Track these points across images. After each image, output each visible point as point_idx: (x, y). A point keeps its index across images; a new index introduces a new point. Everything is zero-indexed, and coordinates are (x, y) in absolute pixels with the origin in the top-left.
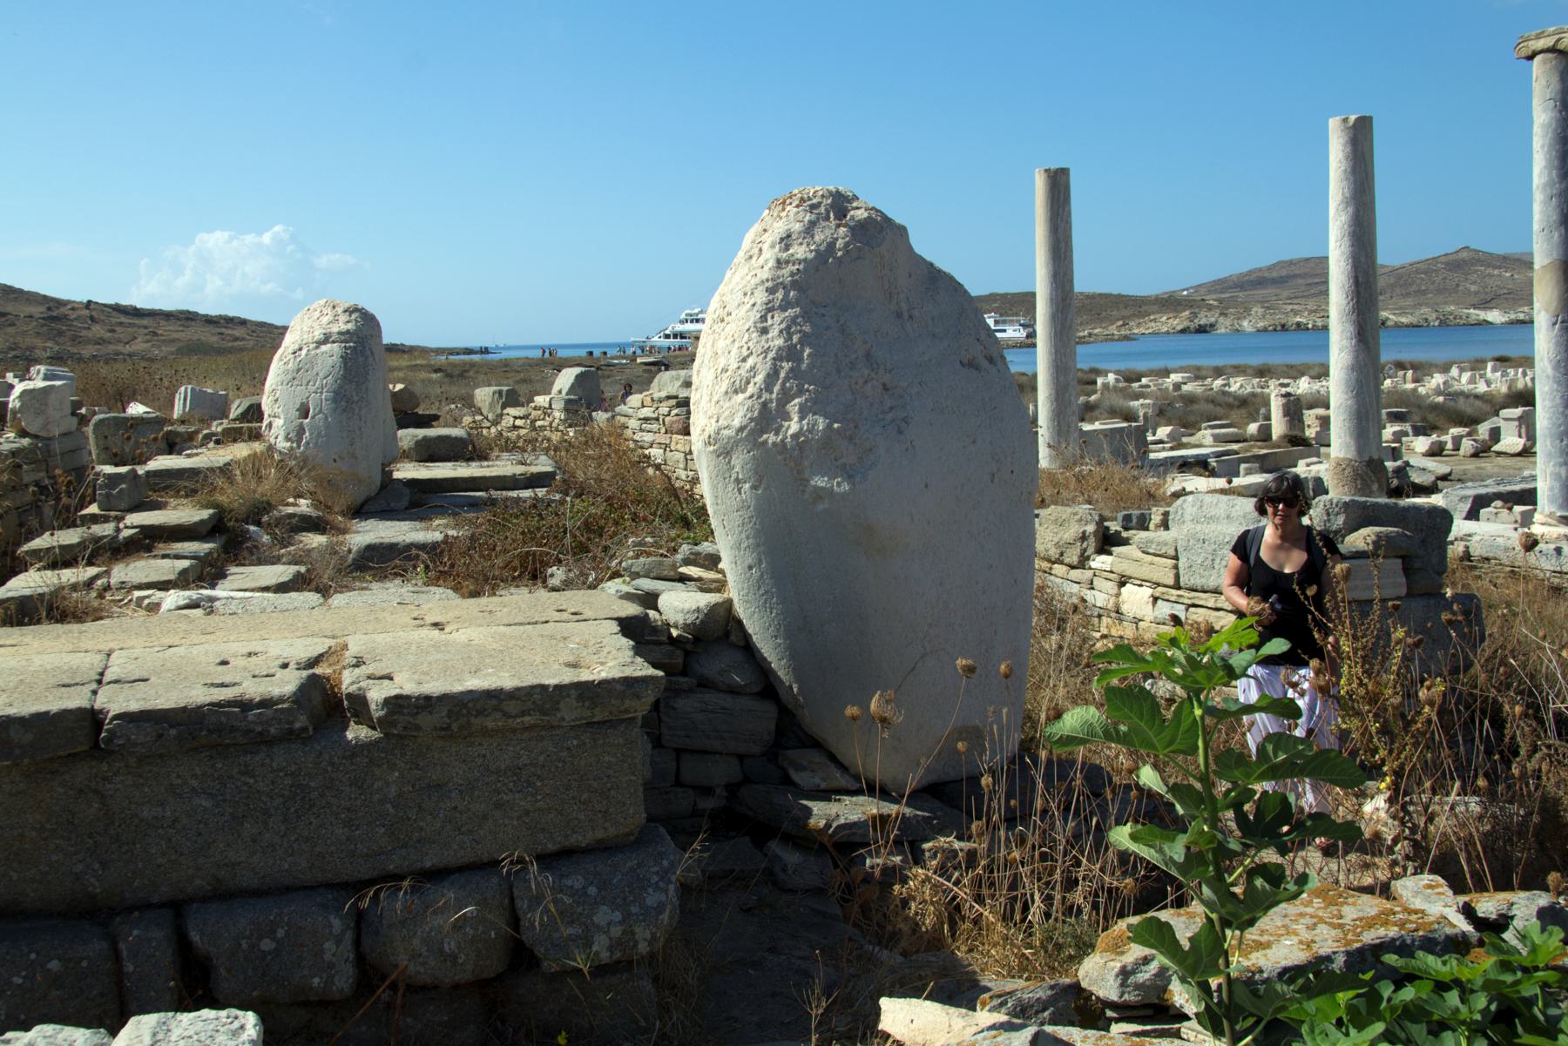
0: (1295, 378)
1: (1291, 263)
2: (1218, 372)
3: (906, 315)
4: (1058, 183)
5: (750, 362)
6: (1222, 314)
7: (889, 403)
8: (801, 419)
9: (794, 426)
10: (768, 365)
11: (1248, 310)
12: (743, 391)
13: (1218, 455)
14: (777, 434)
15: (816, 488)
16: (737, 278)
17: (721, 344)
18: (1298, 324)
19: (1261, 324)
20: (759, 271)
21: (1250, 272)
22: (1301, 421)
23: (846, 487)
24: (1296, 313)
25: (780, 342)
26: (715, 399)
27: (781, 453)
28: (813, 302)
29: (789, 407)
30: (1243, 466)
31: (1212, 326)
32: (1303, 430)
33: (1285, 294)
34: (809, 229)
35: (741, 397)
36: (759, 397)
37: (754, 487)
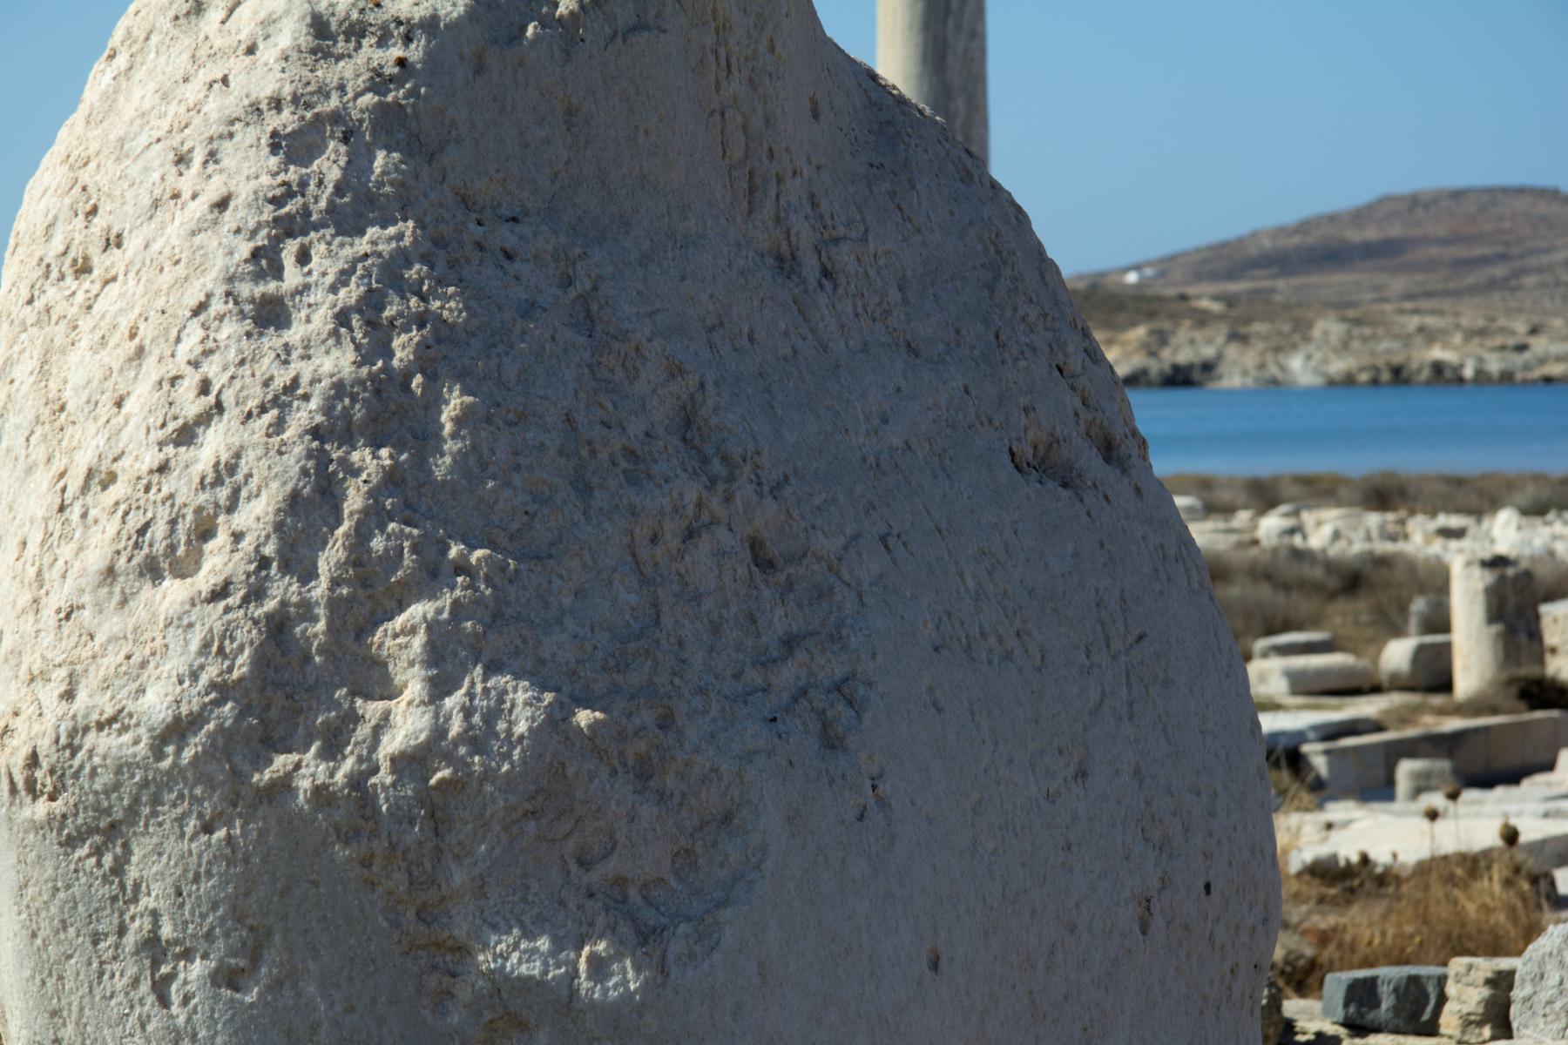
0: (1478, 513)
1: (1415, 202)
2: (1264, 496)
3: (810, 267)
5: (214, 444)
6: (1236, 337)
7: (779, 621)
8: (439, 688)
9: (405, 722)
10: (294, 460)
11: (1302, 328)
12: (182, 571)
13: (1332, 733)
14: (332, 751)
15: (500, 983)
16: (141, 94)
17: (80, 369)
18: (1438, 368)
19: (1338, 366)
20: (236, 66)
21: (1303, 227)
22: (1535, 634)
23: (628, 978)
24: (1429, 336)
25: (339, 362)
26: (57, 598)
27: (348, 836)
28: (465, 201)
29: (384, 638)
30: (1406, 769)
31: (1208, 367)
32: (1541, 661)
33: (1398, 284)
35: (173, 593)
36: (256, 594)
37: (226, 978)
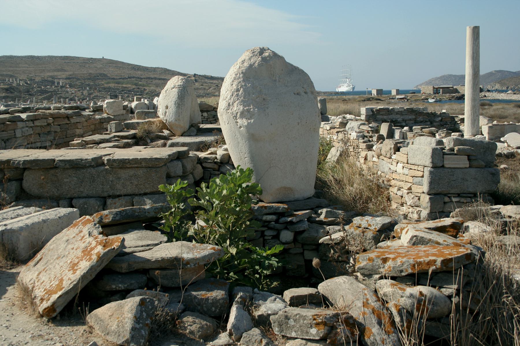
3: (278, 81)
4: (476, 31)
34: (250, 59)
